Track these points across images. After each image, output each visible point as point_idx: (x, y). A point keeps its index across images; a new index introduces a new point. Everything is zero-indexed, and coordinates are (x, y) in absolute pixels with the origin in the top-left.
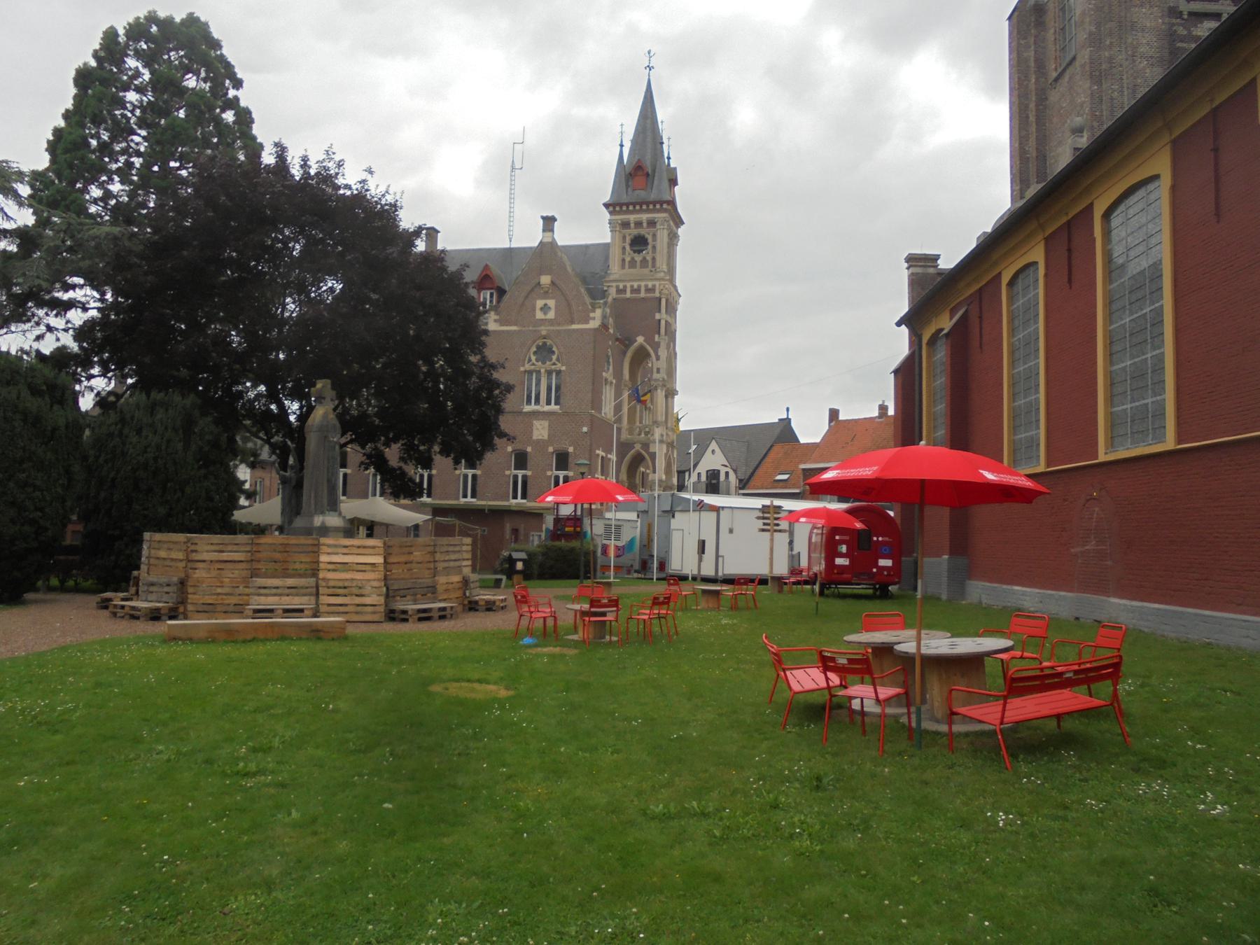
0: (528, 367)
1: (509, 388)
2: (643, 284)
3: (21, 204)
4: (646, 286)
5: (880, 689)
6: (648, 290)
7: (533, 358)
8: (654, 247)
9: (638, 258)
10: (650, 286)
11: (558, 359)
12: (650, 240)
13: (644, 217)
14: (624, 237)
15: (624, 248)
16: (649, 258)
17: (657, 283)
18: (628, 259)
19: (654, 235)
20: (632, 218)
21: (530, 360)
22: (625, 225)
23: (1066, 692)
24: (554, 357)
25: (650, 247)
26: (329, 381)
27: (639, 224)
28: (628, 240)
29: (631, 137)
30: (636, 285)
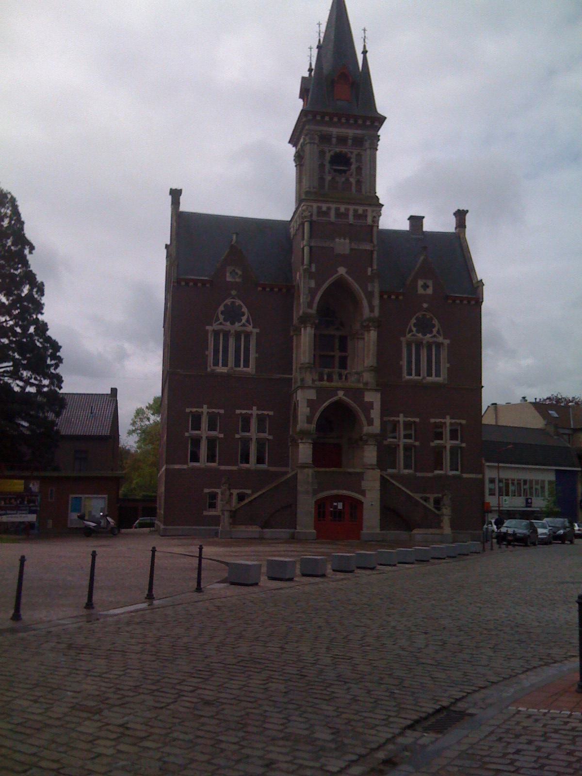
0: (216, 327)
1: (149, 404)
2: (352, 208)
3: (438, 769)
4: (355, 211)
5: (500, 474)
6: (357, 216)
7: (221, 317)
8: (359, 169)
9: (341, 179)
10: (360, 212)
11: (438, 332)
12: (353, 160)
13: (351, 132)
14: (322, 153)
15: (322, 166)
16: (353, 180)
17: (369, 209)
18: (328, 178)
19: (359, 155)
20: (334, 131)
21: (218, 319)
22: (325, 139)
23: (121, 609)
24: (244, 319)
25: (353, 167)
26: (61, 434)
27: (342, 140)
28: (328, 156)
29: (324, 31)
30: (342, 209)
